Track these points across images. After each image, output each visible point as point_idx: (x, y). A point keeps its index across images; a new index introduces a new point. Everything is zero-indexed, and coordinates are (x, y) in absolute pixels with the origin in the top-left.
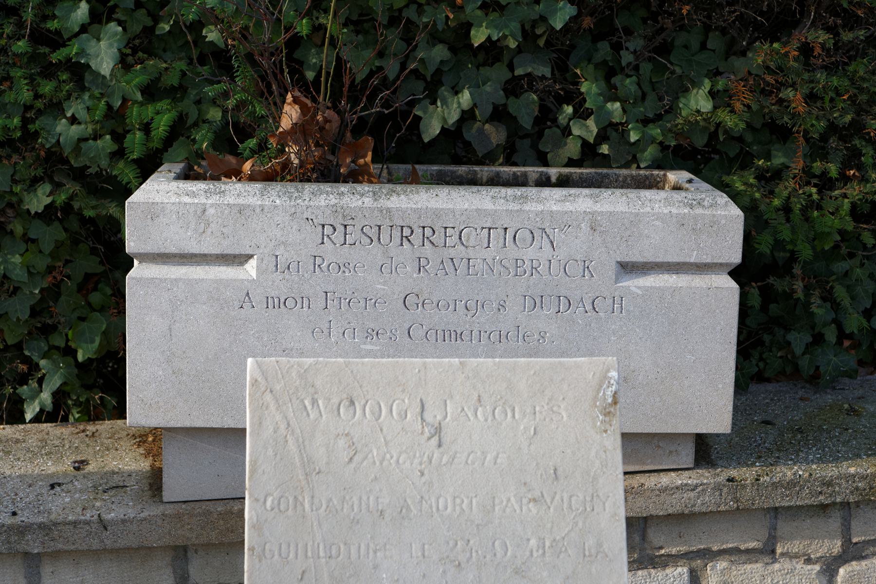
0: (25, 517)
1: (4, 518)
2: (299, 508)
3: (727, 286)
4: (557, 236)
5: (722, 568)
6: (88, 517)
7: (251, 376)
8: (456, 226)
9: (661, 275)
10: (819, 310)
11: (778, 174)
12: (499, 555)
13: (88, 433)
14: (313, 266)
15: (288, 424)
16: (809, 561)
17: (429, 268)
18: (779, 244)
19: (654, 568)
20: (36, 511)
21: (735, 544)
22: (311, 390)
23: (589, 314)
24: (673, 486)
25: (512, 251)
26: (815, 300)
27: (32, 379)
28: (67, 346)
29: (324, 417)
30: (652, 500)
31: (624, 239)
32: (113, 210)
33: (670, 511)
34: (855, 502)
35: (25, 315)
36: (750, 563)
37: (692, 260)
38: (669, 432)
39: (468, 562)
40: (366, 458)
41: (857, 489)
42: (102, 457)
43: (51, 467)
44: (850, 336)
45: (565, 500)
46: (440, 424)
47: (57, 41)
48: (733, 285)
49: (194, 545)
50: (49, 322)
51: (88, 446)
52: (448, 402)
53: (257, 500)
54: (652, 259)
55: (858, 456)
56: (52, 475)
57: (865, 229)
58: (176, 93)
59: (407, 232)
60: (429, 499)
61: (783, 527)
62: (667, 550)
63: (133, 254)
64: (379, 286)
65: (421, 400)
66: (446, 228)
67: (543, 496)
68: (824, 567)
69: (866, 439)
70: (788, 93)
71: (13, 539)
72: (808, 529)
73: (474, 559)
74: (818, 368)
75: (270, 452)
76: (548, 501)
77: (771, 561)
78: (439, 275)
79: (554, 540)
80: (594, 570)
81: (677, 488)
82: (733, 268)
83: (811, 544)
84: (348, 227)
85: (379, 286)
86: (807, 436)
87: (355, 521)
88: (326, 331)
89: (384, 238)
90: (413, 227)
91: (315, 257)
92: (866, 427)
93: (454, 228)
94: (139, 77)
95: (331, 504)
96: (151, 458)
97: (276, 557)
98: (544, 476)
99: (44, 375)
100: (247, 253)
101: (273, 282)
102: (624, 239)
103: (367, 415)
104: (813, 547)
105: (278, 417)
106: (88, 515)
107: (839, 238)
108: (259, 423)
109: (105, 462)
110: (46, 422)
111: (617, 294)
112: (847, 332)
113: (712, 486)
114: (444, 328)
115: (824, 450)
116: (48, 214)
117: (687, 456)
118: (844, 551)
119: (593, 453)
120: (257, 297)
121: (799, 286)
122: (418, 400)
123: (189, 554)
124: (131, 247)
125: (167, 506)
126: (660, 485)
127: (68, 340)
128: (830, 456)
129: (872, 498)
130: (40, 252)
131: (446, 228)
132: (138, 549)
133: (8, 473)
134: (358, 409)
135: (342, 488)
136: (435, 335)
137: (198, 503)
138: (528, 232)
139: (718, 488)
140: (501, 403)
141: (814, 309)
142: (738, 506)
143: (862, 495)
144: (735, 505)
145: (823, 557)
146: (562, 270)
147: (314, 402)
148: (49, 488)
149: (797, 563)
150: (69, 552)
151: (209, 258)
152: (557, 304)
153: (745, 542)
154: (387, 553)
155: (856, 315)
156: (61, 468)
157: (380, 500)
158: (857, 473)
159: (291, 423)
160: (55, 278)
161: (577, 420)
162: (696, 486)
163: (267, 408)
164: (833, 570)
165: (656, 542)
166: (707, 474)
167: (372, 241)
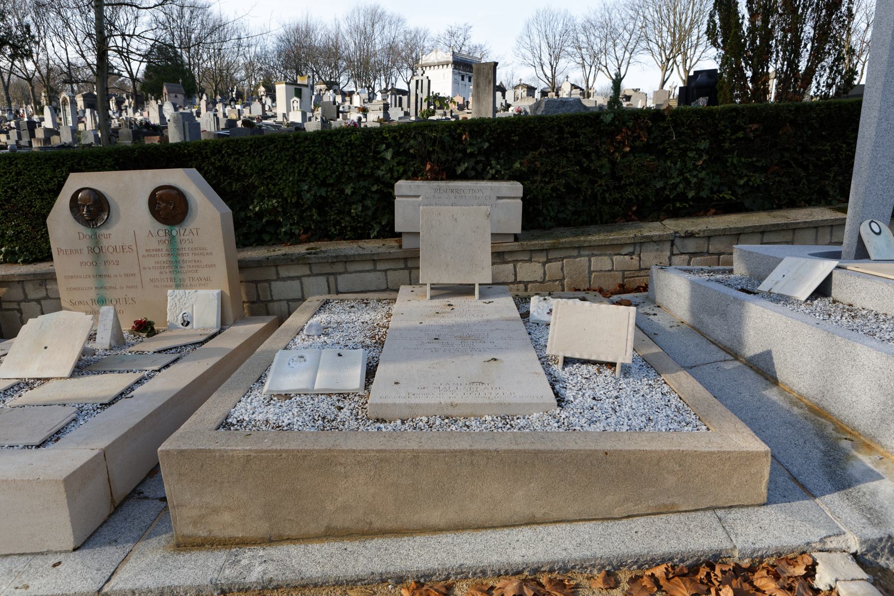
0: (374, 252)
10: (544, 211)
11: (535, 181)
32: (390, 190)
47: (379, 153)
58: (404, 164)
61: (534, 255)
68: (414, 124)
70: (537, 163)
94: (396, 160)
116: (376, 192)
117: (512, 239)
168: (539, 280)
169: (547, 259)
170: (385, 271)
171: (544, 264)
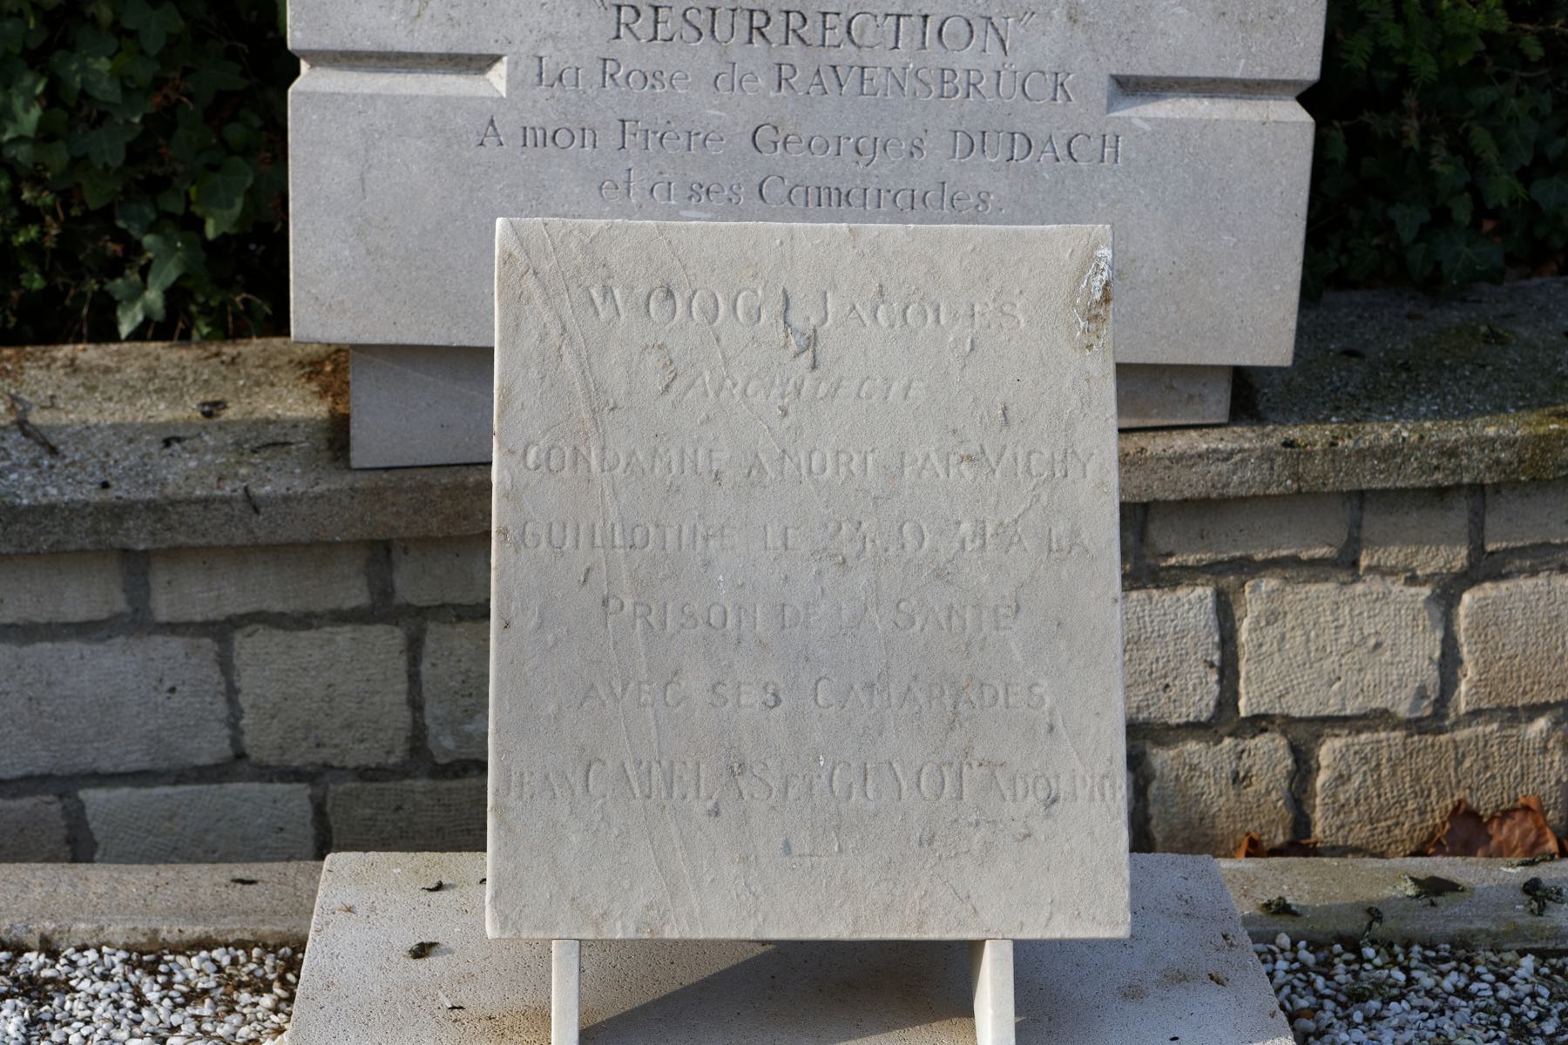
0: (122, 491)
1: (89, 491)
2: (581, 465)
3: (1294, 119)
4: (1011, 29)
5: (1269, 588)
6: (227, 489)
7: (502, 247)
8: (843, 10)
9: (1184, 100)
10: (1443, 166)
12: (908, 547)
13: (224, 358)
14: (601, 76)
15: (564, 328)
16: (1413, 580)
17: (796, 82)
18: (1381, 55)
19: (1158, 587)
20: (141, 481)
21: (1293, 551)
22: (602, 272)
23: (1062, 163)
24: (1193, 452)
25: (935, 55)
26: (1439, 151)
27: (130, 268)
28: (188, 212)
29: (623, 317)
30: (1158, 475)
31: (1124, 37)
33: (1187, 494)
34: (1494, 484)
35: (117, 159)
36: (1316, 582)
37: (1237, 75)
38: (1189, 362)
39: (858, 557)
40: (691, 385)
41: (1498, 462)
42: (249, 396)
43: (163, 412)
44: (1494, 214)
45: (1019, 460)
46: (815, 331)
48: (1304, 118)
49: (403, 540)
50: (159, 171)
51: (225, 378)
52: (829, 295)
53: (512, 452)
54: (1169, 72)
55: (1502, 409)
56: (167, 425)
57: (1526, 31)
59: (759, 20)
60: (796, 454)
61: (1373, 523)
62: (1180, 559)
63: (300, 51)
64: (712, 112)
65: (784, 291)
66: (825, 14)
67: (983, 452)
68: (1438, 591)
69: (1515, 381)
71: (104, 526)
72: (1414, 527)
73: (868, 553)
74: (1438, 265)
75: (534, 374)
76: (992, 460)
77: (1350, 579)
78: (812, 95)
79: (1001, 524)
80: (1064, 573)
81: (1200, 456)
82: (1304, 89)
83: (1417, 552)
84: (660, 10)
85: (712, 112)
86: (1418, 375)
87: (674, 488)
88: (622, 187)
89: (722, 30)
90: (770, 12)
91: (605, 60)
92: (1515, 362)
93: (838, 14)
95: (634, 460)
96: (330, 399)
97: (544, 544)
98: (986, 420)
99: (150, 262)
100: (491, 52)
101: (535, 101)
102: (1124, 37)
103: (694, 314)
104: (1421, 557)
105: (547, 316)
106: (228, 488)
107: (1481, 46)
108: (514, 327)
109: (254, 405)
110: (155, 338)
111: (1109, 130)
112: (1490, 206)
113: (1259, 452)
114: (819, 184)
115: (1444, 399)
117: (1217, 404)
118: (1472, 566)
119: (1068, 383)
120: (508, 126)
121: (1412, 126)
122: (780, 291)
123: (394, 555)
124: (296, 37)
125: (359, 475)
126: (1171, 451)
127: (189, 203)
128: (1455, 408)
129: (1523, 478)
130: (142, 52)
131: (825, 14)
132: (309, 546)
133: (93, 420)
134: (679, 305)
135: (653, 434)
136: (803, 195)
137: (409, 471)
138: (963, 24)
139: (1267, 456)
140: (916, 297)
141: (1436, 166)
142: (1299, 489)
143: (1505, 472)
144: (1295, 486)
145: (1435, 574)
146: (1019, 88)
147: (607, 291)
148: (162, 445)
149: (1394, 583)
150: (195, 549)
151: (428, 60)
152: (1009, 145)
153: (1309, 547)
154: (726, 541)
155: (1506, 177)
156: (180, 414)
157: (715, 455)
158: (1499, 436)
159: (568, 326)
160: (166, 97)
161: (1042, 328)
162: (1231, 454)
163: (528, 301)
164: (1453, 596)
165: (1163, 547)
166: (1249, 435)
167: (701, 34)
168: (1403, 710)
169: (1477, 550)
170: (221, 630)
171: (1447, 593)
